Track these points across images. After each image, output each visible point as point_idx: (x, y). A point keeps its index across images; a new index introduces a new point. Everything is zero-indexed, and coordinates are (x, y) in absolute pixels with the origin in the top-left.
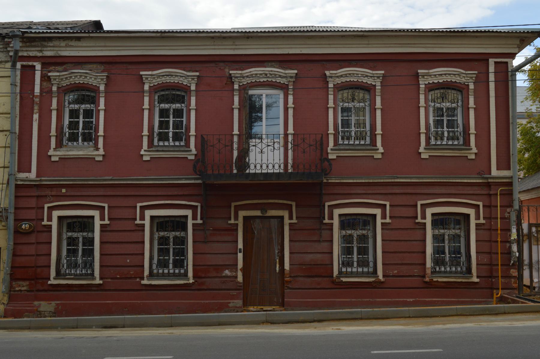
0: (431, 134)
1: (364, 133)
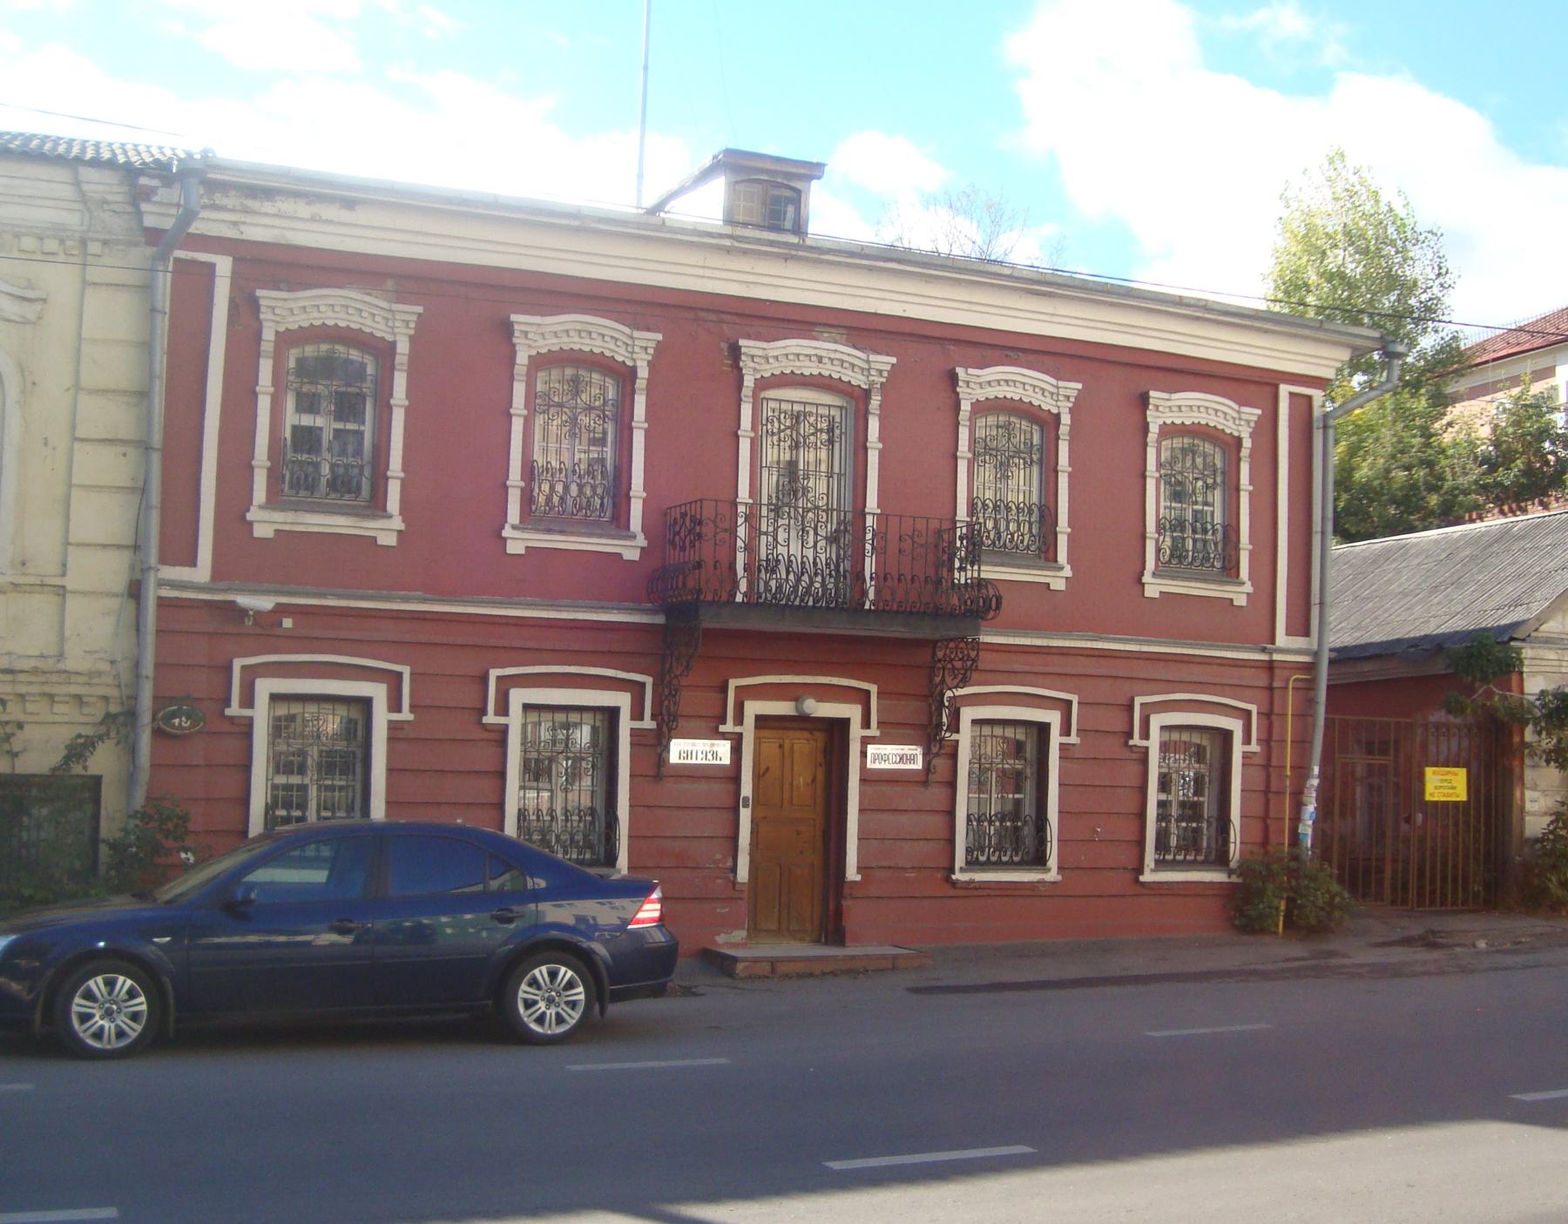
1: (356, 471)
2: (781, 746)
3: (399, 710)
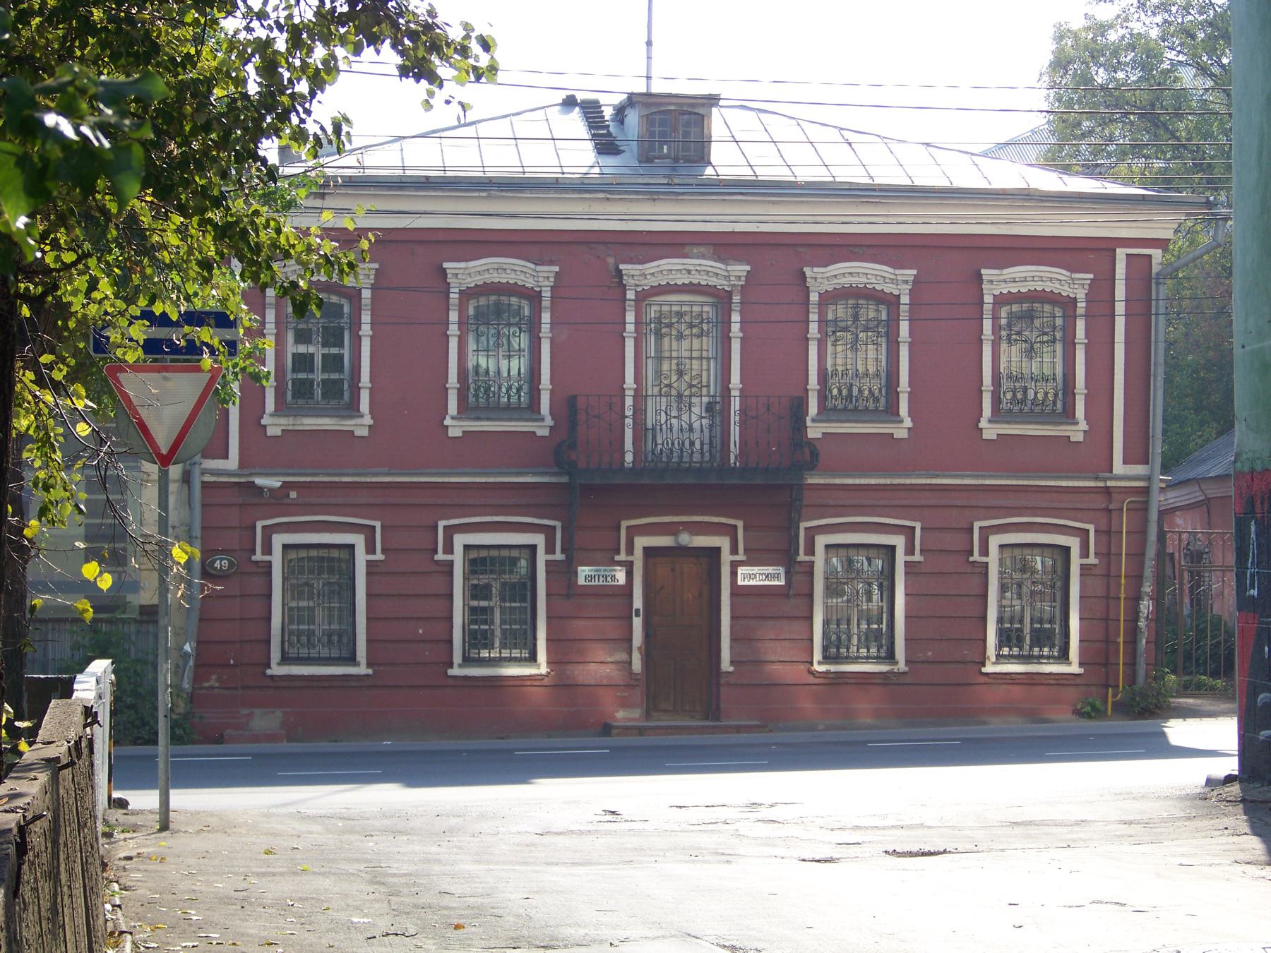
2: (673, 570)
3: (374, 552)
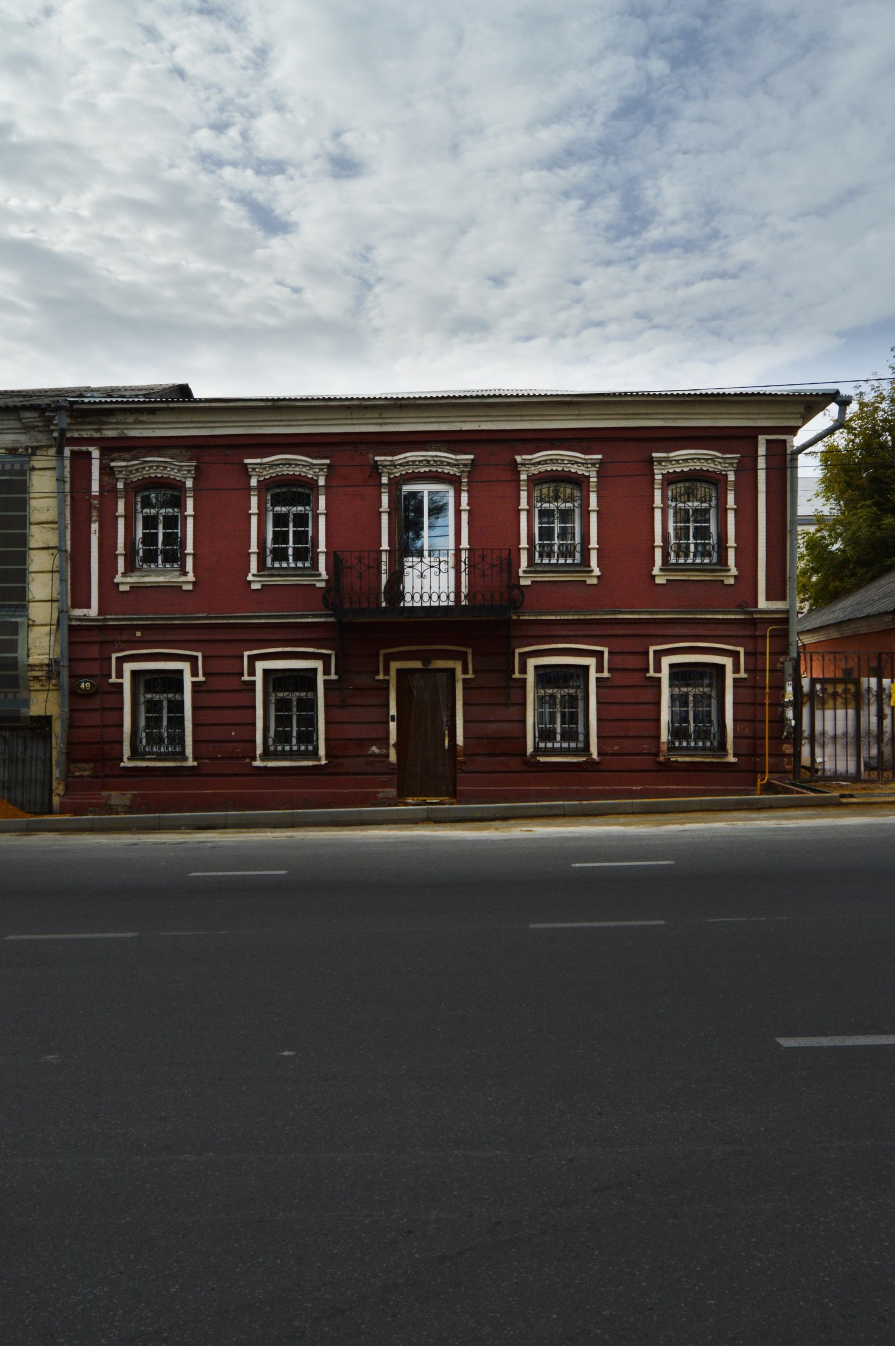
0: (670, 549)
